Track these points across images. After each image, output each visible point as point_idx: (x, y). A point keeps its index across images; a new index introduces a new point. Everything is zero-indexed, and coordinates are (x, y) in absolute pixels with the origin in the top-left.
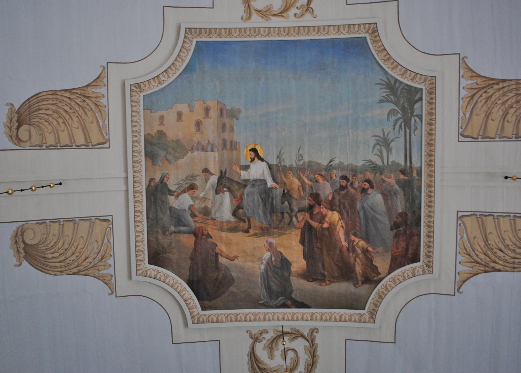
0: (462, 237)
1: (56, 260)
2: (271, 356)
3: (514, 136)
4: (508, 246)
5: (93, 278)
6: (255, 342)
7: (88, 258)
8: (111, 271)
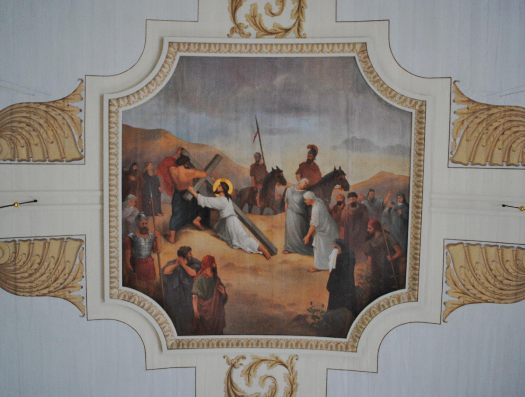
0: (80, 137)
1: (26, 280)
2: (249, 382)
3: (32, 242)
4: (34, 130)
5: (62, 300)
6: (231, 368)
7: (479, 123)
8: (455, 107)
